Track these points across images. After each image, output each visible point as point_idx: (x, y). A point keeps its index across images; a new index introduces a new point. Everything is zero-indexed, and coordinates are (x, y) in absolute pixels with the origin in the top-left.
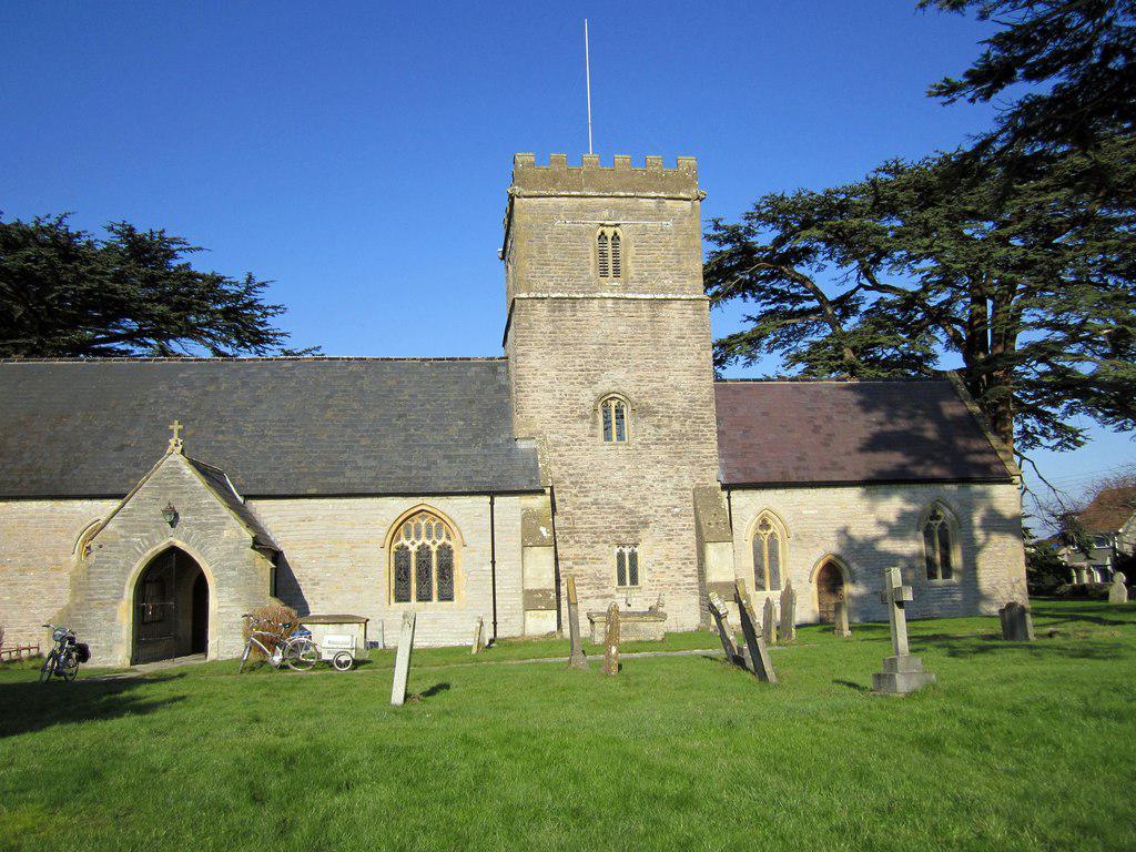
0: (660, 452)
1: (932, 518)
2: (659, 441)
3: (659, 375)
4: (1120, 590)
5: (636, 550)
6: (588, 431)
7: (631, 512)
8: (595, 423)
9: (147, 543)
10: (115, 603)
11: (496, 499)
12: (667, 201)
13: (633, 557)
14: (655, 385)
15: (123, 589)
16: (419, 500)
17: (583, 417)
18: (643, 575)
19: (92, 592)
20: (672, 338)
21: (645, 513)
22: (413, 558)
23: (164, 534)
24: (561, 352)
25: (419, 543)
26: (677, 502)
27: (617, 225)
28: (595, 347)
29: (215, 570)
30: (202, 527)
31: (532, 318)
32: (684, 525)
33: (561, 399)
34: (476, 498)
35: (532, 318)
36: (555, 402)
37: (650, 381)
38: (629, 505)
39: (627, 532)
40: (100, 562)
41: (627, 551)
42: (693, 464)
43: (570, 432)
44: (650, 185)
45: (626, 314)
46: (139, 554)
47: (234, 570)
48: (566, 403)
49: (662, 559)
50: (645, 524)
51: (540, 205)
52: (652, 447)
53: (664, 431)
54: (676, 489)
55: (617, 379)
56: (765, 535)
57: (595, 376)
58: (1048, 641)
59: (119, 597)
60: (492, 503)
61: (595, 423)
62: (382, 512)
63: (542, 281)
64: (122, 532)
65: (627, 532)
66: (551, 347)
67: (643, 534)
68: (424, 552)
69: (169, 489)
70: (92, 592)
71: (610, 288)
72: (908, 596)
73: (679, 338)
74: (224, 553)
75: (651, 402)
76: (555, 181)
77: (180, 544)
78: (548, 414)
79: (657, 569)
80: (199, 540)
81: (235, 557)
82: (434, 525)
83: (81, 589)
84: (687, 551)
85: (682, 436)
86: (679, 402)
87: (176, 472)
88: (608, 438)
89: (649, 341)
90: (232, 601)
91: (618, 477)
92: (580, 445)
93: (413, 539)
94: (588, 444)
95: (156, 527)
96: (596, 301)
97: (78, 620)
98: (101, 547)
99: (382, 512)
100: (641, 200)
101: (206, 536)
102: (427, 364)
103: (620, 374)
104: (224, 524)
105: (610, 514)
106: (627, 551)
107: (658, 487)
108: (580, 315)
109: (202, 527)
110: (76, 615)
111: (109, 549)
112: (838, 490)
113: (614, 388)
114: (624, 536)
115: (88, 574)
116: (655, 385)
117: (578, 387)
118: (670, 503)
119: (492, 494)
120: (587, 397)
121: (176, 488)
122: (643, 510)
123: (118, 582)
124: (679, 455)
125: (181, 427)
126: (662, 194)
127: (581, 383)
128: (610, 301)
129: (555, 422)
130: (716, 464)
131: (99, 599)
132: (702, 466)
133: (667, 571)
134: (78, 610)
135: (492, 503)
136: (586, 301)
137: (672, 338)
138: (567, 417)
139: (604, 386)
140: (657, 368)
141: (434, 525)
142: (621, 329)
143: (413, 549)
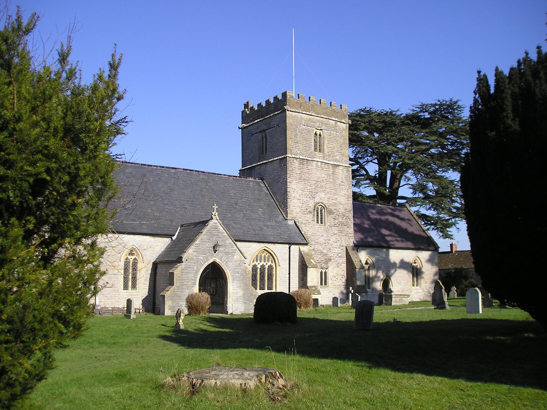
0: (335, 230)
1: (130, 254)
2: (335, 225)
3: (335, 197)
4: (454, 293)
5: (327, 270)
6: (312, 219)
7: (325, 255)
8: (314, 215)
9: (205, 260)
10: (193, 287)
11: (293, 247)
12: (338, 123)
13: (325, 273)
14: (334, 201)
15: (196, 280)
16: (266, 245)
17: (310, 212)
18: (329, 281)
19: (183, 281)
20: (339, 182)
21: (330, 255)
22: (259, 270)
23: (212, 256)
24: (303, 183)
25: (261, 264)
26: (340, 251)
27: (321, 130)
28: (314, 182)
29: (231, 274)
30: (227, 253)
31: (293, 166)
32: (343, 261)
33: (303, 204)
34: (284, 245)
35: (293, 166)
36: (301, 205)
37: (332, 199)
38: (325, 251)
39: (325, 263)
40: (187, 267)
41: (324, 271)
42: (345, 235)
43: (306, 218)
44: (333, 114)
45: (325, 169)
46: (202, 264)
47: (238, 273)
48: (304, 206)
49: (335, 275)
50: (330, 260)
51: (295, 116)
52: (333, 227)
53: (337, 221)
54: (340, 246)
55: (321, 197)
56: (131, 258)
57: (314, 194)
58: (117, 328)
59: (195, 284)
60: (290, 248)
61: (314, 215)
62: (250, 249)
63: (296, 150)
64: (195, 254)
65: (325, 263)
66: (300, 180)
67: (330, 264)
68: (263, 266)
69: (214, 235)
70: (183, 281)
71: (318, 156)
72: (352, 292)
73: (341, 182)
74: (235, 265)
75: (332, 208)
76: (301, 106)
77: (218, 261)
78: (298, 210)
79: (333, 279)
80: (225, 260)
81: (239, 268)
82: (267, 256)
83: (179, 280)
84: (343, 272)
85: (342, 224)
86: (342, 210)
87: (216, 228)
88: (318, 223)
89: (332, 182)
90: (238, 287)
91: (321, 240)
92: (309, 224)
93: (259, 262)
94: (311, 224)
95: (209, 252)
96: (315, 162)
97: (178, 294)
98: (187, 260)
99: (250, 249)
100: (330, 120)
101: (228, 257)
102: (231, 178)
103: (322, 195)
104: (235, 253)
105: (319, 255)
106: (324, 271)
107: (335, 244)
108: (309, 167)
109: (227, 253)
110: (177, 292)
111: (190, 261)
112: (399, 250)
113: (321, 201)
114: (323, 264)
115: (182, 272)
116: (334, 201)
117: (308, 199)
118: (338, 252)
119: (290, 244)
120: (311, 204)
121: (216, 235)
122: (330, 254)
123: (193, 277)
124: (341, 232)
125: (217, 207)
126: (337, 119)
127: (310, 198)
128: (319, 163)
129: (301, 214)
130: (353, 237)
131: (187, 285)
132: (348, 237)
133: (337, 280)
134: (177, 289)
135: (290, 248)
136: (311, 162)
137: (339, 182)
138: (305, 212)
139: (317, 200)
140: (335, 194)
141: (267, 256)
142: (323, 175)
143: (259, 266)
